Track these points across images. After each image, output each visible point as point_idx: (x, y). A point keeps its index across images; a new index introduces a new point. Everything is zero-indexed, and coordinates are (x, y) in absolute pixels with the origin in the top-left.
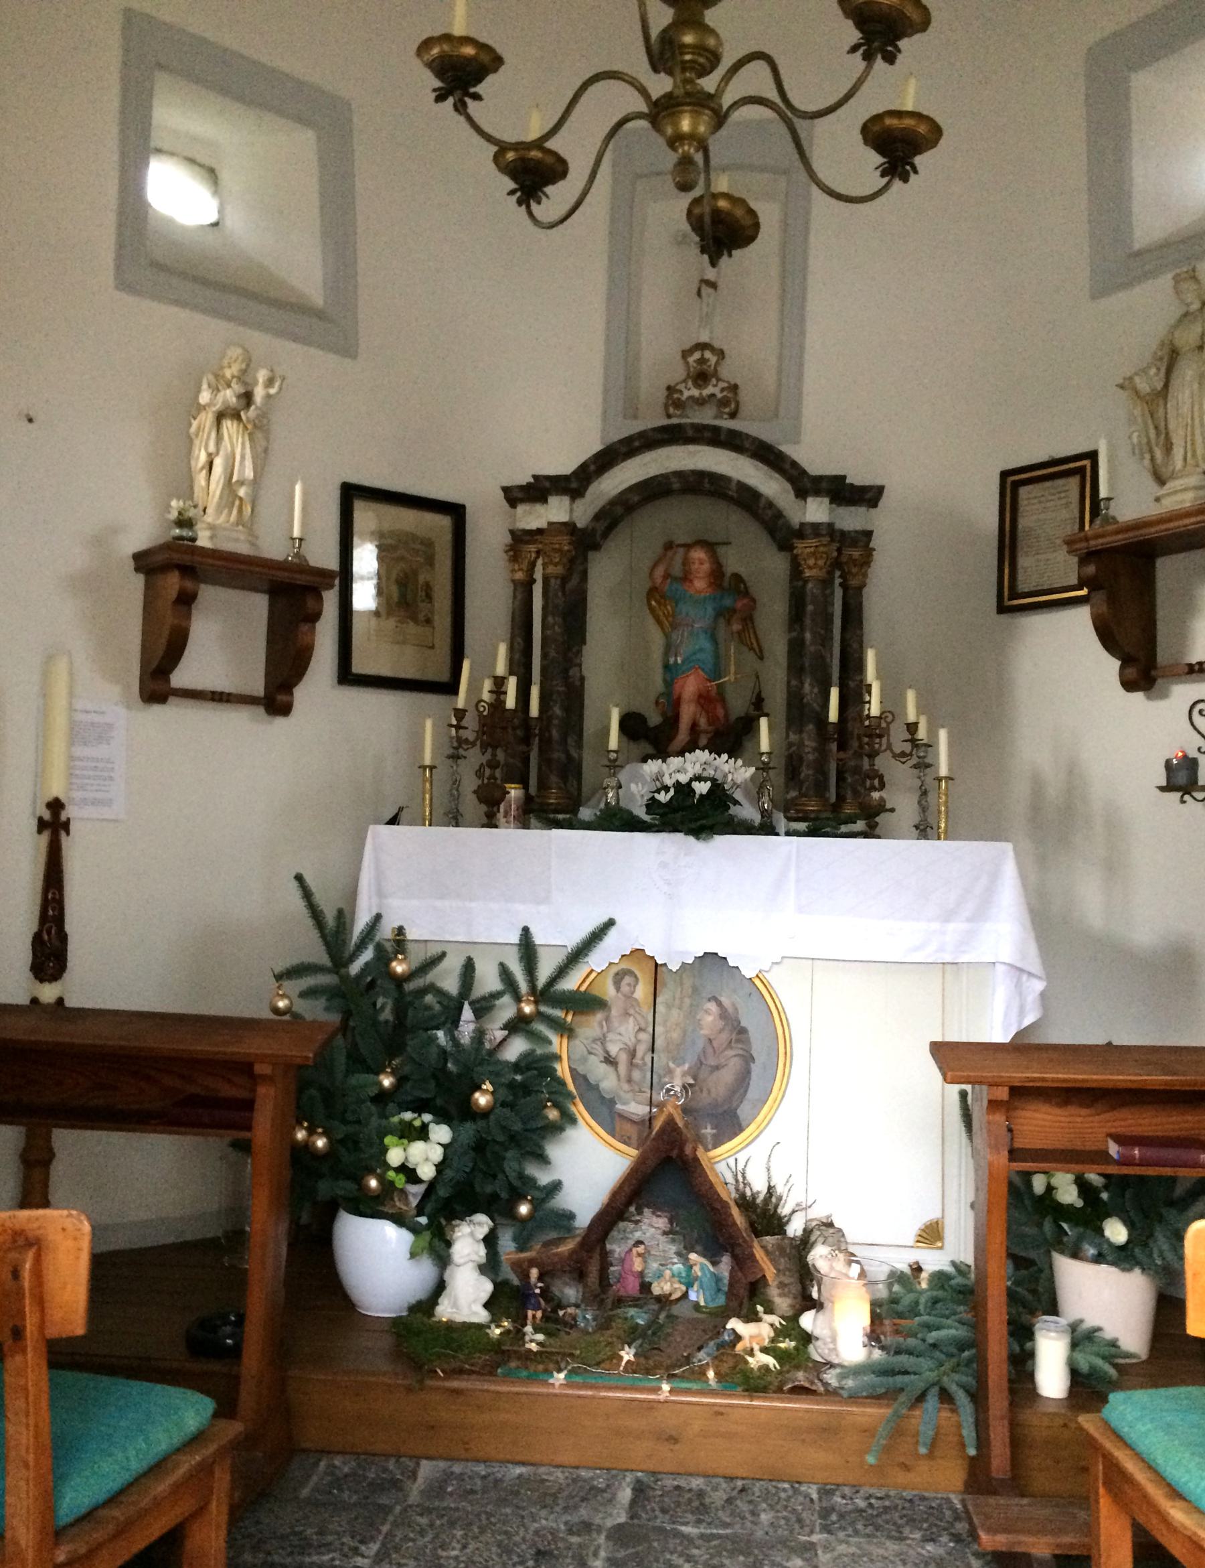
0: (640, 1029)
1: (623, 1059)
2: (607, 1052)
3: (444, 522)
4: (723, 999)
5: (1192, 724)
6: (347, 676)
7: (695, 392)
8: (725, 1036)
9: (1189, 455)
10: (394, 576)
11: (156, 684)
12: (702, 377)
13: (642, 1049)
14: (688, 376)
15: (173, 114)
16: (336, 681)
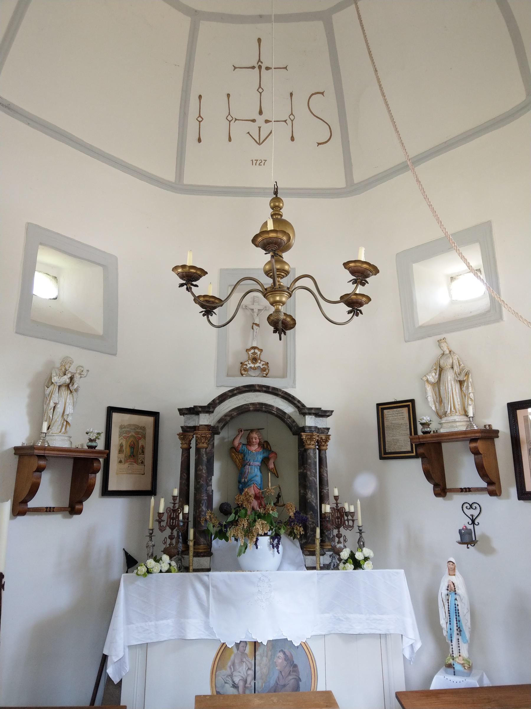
0: (249, 669)
1: (241, 684)
2: (234, 682)
3: (150, 420)
4: (286, 650)
5: (463, 510)
6: (106, 492)
7: (252, 365)
8: (287, 669)
9: (452, 408)
10: (129, 444)
11: (20, 509)
12: (255, 360)
13: (249, 679)
14: (249, 359)
15: (45, 257)
16: (101, 494)
